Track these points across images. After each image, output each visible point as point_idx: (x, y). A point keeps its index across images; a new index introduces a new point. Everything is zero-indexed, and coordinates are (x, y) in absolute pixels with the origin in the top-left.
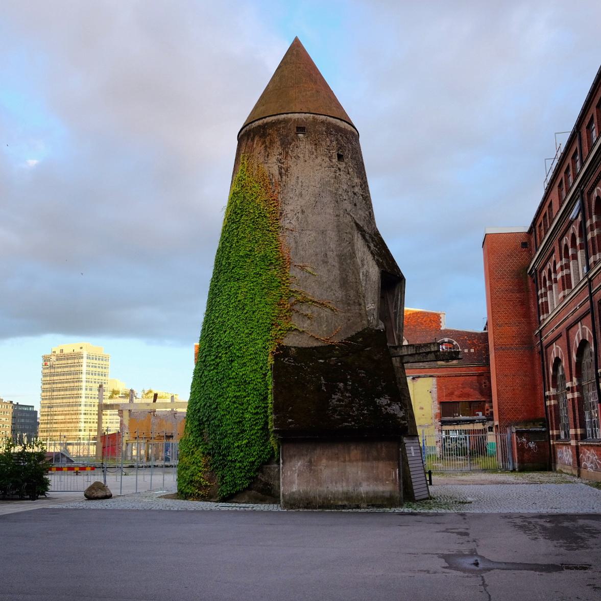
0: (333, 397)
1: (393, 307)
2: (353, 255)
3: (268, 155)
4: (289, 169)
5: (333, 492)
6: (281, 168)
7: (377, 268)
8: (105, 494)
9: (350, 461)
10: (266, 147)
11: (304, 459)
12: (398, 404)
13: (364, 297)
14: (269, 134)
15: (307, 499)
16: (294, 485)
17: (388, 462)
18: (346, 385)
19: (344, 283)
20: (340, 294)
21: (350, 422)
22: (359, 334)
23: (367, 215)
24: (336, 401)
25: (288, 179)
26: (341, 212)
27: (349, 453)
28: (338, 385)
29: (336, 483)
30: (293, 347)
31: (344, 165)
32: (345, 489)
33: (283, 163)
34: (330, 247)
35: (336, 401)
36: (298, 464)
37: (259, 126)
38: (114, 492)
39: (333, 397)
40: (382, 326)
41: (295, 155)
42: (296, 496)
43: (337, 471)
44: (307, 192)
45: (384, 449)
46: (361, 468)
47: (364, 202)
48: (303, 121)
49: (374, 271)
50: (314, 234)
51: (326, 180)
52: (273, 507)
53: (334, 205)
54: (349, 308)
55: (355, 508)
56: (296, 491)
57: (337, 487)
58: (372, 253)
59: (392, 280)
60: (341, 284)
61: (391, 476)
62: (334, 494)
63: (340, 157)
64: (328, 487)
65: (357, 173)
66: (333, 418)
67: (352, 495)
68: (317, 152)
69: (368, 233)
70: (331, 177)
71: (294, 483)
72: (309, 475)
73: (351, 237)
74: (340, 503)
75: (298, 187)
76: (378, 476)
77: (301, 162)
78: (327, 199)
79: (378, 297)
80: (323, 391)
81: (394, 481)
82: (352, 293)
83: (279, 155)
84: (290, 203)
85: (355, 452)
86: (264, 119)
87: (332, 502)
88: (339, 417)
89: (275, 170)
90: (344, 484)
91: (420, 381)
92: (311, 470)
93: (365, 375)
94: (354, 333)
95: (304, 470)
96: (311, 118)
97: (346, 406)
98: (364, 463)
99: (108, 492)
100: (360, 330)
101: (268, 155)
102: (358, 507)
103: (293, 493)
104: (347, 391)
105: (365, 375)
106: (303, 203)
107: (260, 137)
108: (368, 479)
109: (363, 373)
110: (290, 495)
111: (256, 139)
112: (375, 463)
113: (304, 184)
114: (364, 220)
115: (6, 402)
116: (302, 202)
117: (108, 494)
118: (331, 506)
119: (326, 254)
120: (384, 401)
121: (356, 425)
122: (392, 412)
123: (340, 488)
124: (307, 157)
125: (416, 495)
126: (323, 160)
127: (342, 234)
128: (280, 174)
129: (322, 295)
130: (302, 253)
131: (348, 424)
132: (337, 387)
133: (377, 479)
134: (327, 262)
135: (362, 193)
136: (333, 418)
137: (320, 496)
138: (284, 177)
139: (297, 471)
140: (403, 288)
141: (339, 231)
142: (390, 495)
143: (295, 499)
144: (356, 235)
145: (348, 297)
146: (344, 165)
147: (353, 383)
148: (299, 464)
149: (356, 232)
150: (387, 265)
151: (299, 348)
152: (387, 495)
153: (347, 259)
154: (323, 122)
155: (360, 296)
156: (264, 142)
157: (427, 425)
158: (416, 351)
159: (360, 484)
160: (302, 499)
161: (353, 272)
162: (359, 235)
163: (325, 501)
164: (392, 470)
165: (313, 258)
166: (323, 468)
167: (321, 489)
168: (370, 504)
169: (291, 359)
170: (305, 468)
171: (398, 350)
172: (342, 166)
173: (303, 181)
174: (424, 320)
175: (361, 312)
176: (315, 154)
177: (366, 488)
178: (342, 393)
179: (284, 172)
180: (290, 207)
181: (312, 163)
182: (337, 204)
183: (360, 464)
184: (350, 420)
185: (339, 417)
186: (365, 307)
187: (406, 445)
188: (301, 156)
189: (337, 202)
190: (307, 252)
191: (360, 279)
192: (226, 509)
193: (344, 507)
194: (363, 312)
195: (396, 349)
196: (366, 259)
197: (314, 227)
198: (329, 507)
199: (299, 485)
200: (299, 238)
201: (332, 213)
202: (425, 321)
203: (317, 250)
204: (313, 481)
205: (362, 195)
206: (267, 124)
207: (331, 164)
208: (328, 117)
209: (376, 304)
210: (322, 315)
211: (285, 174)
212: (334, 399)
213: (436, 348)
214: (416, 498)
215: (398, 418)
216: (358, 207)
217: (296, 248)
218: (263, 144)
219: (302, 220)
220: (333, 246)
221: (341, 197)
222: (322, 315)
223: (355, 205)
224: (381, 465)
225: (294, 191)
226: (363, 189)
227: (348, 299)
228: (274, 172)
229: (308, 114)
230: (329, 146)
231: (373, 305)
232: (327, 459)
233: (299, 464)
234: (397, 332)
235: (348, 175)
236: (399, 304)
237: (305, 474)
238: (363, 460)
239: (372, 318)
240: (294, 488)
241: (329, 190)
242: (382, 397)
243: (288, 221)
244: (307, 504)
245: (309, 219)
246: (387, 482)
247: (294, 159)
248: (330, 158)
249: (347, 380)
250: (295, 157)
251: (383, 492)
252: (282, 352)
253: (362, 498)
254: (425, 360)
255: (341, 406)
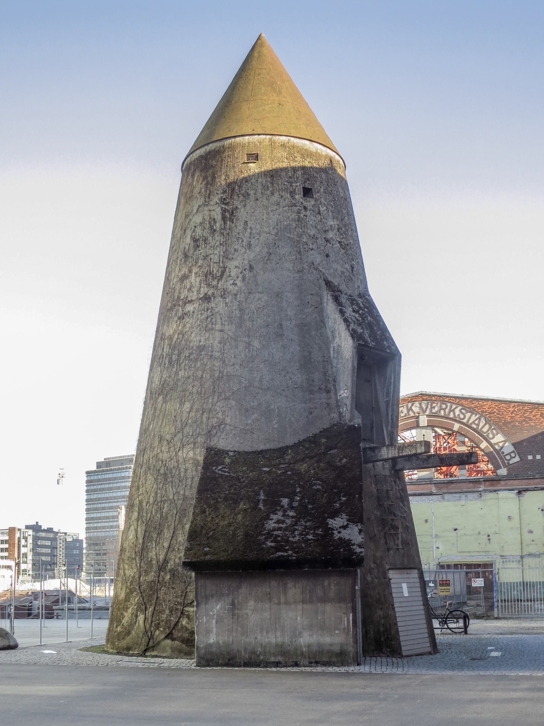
0: (271, 518)
1: (385, 394)
2: (322, 323)
3: (209, 195)
4: (235, 212)
5: (264, 644)
6: (224, 211)
7: (350, 341)
8: (7, 644)
9: (287, 603)
10: (207, 184)
11: (225, 601)
12: (357, 526)
13: (335, 381)
14: (212, 166)
15: (228, 653)
16: (211, 635)
17: (338, 605)
18: (292, 500)
19: (306, 363)
20: (299, 378)
21: (286, 551)
22: (325, 432)
23: (347, 269)
24: (274, 523)
25: (233, 225)
26: (305, 266)
27: (285, 592)
28: (281, 501)
29: (267, 632)
30: (231, 451)
31: (313, 202)
32: (280, 640)
33: (227, 204)
34: (287, 315)
35: (274, 523)
36: (217, 607)
37: (201, 156)
38: (21, 641)
39: (271, 518)
40: (358, 421)
41: (243, 192)
42: (214, 649)
43: (268, 617)
44: (257, 242)
45: (333, 587)
46: (301, 612)
47: (343, 251)
48: (255, 145)
49: (345, 345)
50: (265, 298)
51: (285, 223)
52: (189, 663)
53: (294, 257)
54: (312, 396)
55: (292, 666)
56: (214, 643)
57: (268, 638)
58: (346, 320)
59: (377, 356)
60: (301, 365)
61: (343, 624)
62: (265, 647)
63: (307, 192)
64: (256, 638)
65: (332, 212)
66: (264, 546)
67: (288, 648)
68: (273, 187)
69: (346, 294)
70: (294, 220)
71: (212, 632)
72: (231, 621)
73: (319, 300)
74: (272, 659)
75: (246, 235)
76: (324, 623)
77: (251, 203)
78: (284, 250)
79: (352, 381)
80: (260, 509)
81: (346, 631)
82: (317, 376)
83: (223, 193)
84: (234, 257)
85: (294, 589)
86: (206, 147)
87: (262, 657)
88: (272, 544)
89: (217, 215)
90: (278, 634)
91: (528, 494)
92: (233, 615)
93: (320, 488)
94: (317, 431)
95: (224, 616)
96: (267, 142)
97: (286, 529)
98: (305, 606)
99: (12, 640)
100: (326, 425)
101: (209, 195)
102: (296, 665)
103: (211, 645)
104: (292, 508)
105: (320, 488)
106: (252, 256)
107: (201, 171)
108: (310, 627)
109: (319, 484)
110: (206, 648)
111: (197, 174)
112: (320, 606)
113: (254, 231)
114: (341, 277)
115: (46, 529)
116: (251, 255)
117: (11, 644)
118: (260, 663)
119: (281, 325)
120: (336, 523)
121: (294, 555)
122: (347, 537)
123: (272, 639)
124: (259, 195)
125: (403, 648)
126: (282, 196)
127: (305, 296)
128: (224, 218)
129: (272, 379)
130: (248, 324)
131: (283, 554)
132: (279, 503)
133: (322, 628)
134: (282, 335)
135: (338, 239)
136: (264, 546)
137: (245, 650)
138: (228, 222)
139: (215, 616)
140: (397, 367)
141: (301, 293)
142: (341, 650)
143: (211, 653)
144: (325, 298)
145: (310, 382)
146: (313, 202)
147: (302, 498)
148: (218, 607)
149: (325, 293)
150: (370, 337)
151: (239, 453)
152: (337, 649)
153: (312, 331)
154: (283, 145)
155: (328, 380)
156: (205, 178)
157: (538, 553)
158: (398, 453)
159: (300, 633)
160: (222, 654)
161: (320, 348)
162: (330, 297)
163: (253, 657)
164: (343, 615)
165: (262, 330)
166: (250, 613)
167: (248, 640)
168: (313, 660)
169: (225, 468)
170: (226, 612)
171: (376, 452)
172: (310, 203)
173: (253, 226)
174: (533, 414)
175: (329, 401)
176: (271, 189)
177: (307, 639)
178: (285, 511)
179: (228, 216)
180: (235, 263)
181: (265, 202)
182: (299, 256)
183: (300, 607)
184: (287, 548)
185: (272, 544)
186: (336, 394)
187: (392, 581)
188: (252, 192)
189: (300, 253)
190: (255, 322)
191: (330, 357)
192: (135, 666)
193: (277, 664)
194: (333, 402)
195: (374, 451)
196: (338, 329)
197: (266, 288)
198: (257, 665)
199: (217, 635)
200: (244, 304)
201: (291, 269)
202: (534, 416)
203: (269, 320)
204: (237, 629)
205: (340, 242)
206: (210, 152)
207: (293, 202)
208: (292, 139)
209: (350, 390)
210: (272, 407)
211: (230, 218)
212: (272, 519)
213: (423, 448)
214: (404, 653)
215: (353, 545)
216: (332, 258)
217: (241, 318)
218: (203, 181)
219: (249, 279)
220: (290, 313)
221: (306, 246)
222: (272, 407)
223: (327, 256)
224: (328, 608)
225: (240, 240)
226: (342, 234)
227: (311, 385)
228: (216, 217)
229: (262, 136)
230: (290, 177)
231: (346, 391)
232: (255, 601)
233: (218, 607)
234: (389, 428)
235: (318, 216)
236: (392, 390)
237: (226, 621)
238: (303, 602)
239: (345, 409)
240: (212, 639)
241: (289, 237)
242: (337, 517)
243: (231, 282)
244: (229, 660)
245: (259, 278)
246: (337, 632)
247: (241, 198)
248: (292, 193)
249: (295, 494)
250: (243, 195)
251: (331, 645)
252: (214, 456)
253: (302, 654)
254: (426, 466)
255: (280, 529)
